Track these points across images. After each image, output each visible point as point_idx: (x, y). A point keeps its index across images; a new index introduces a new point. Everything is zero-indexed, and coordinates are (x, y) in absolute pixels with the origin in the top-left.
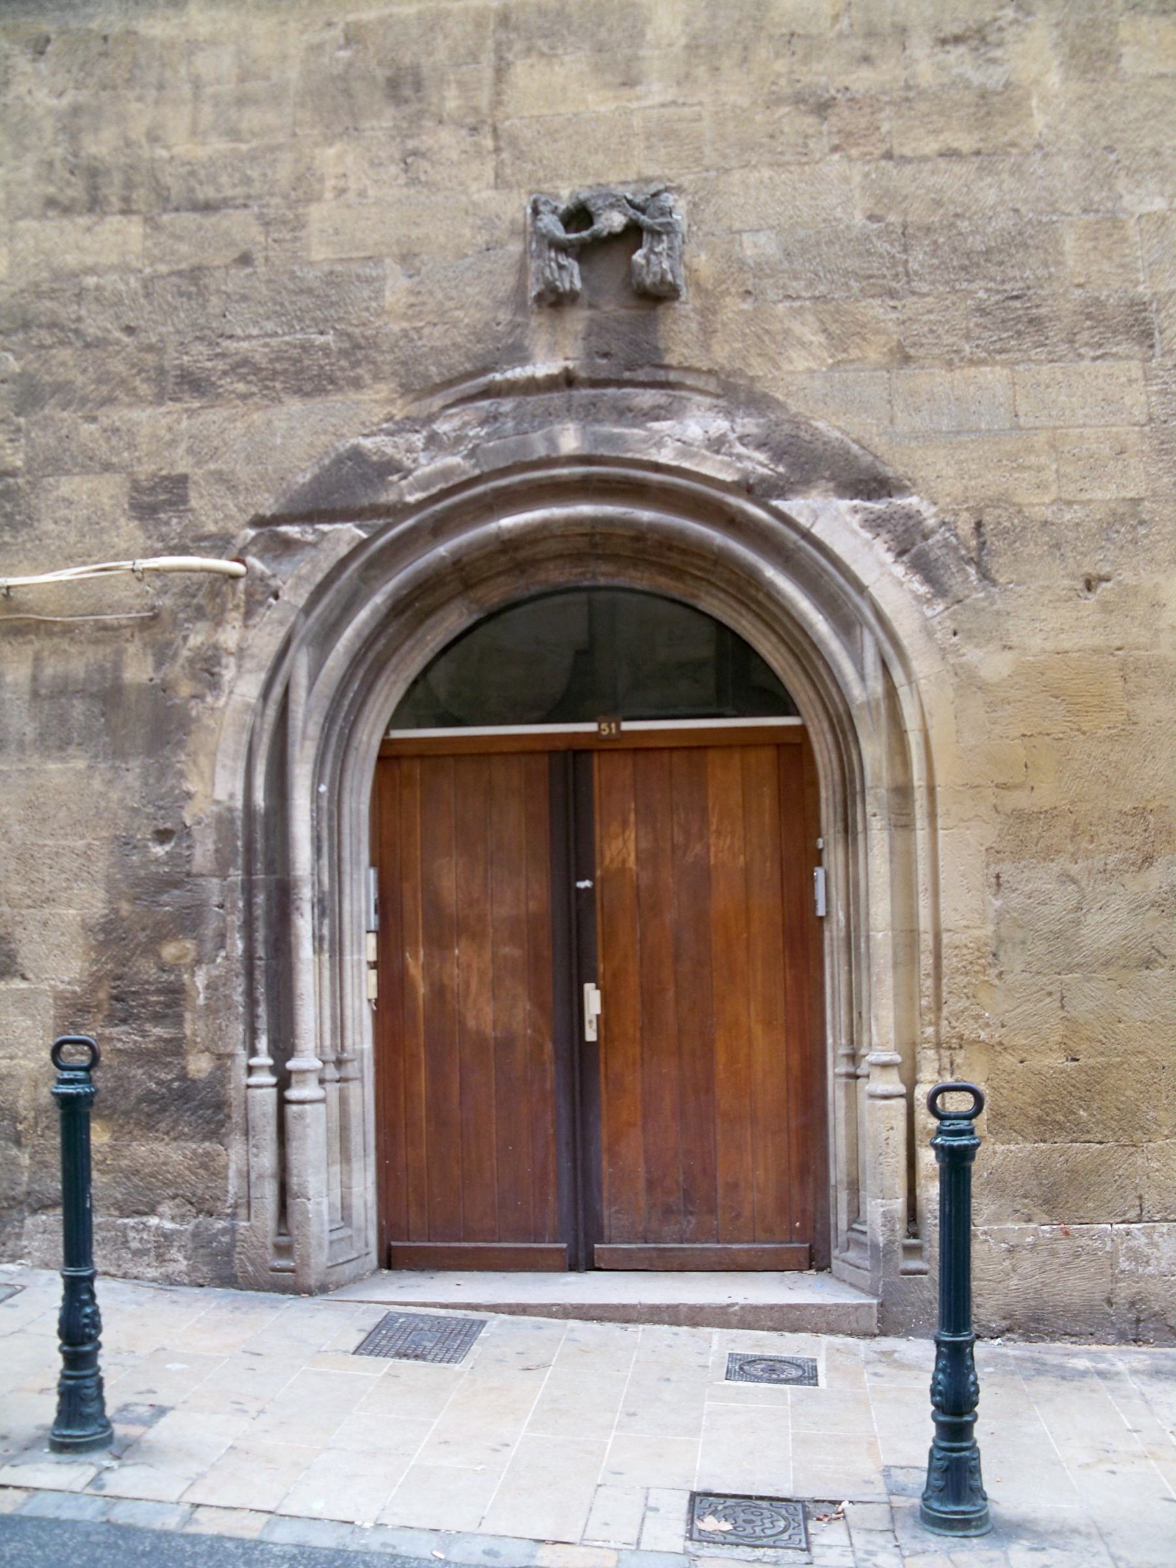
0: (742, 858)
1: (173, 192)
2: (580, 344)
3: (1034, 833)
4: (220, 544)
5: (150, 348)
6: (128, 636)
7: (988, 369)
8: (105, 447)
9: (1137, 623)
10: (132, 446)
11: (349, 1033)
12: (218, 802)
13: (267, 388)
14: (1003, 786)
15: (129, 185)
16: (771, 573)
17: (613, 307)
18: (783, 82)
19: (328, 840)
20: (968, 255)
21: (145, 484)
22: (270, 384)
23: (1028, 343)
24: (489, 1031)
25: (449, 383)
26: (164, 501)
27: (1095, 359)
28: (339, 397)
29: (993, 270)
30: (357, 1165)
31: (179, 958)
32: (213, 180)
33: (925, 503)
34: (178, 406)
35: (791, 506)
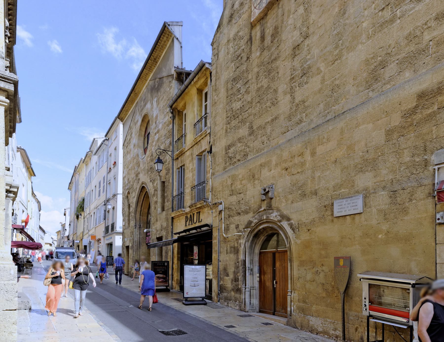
19: (252, 262)
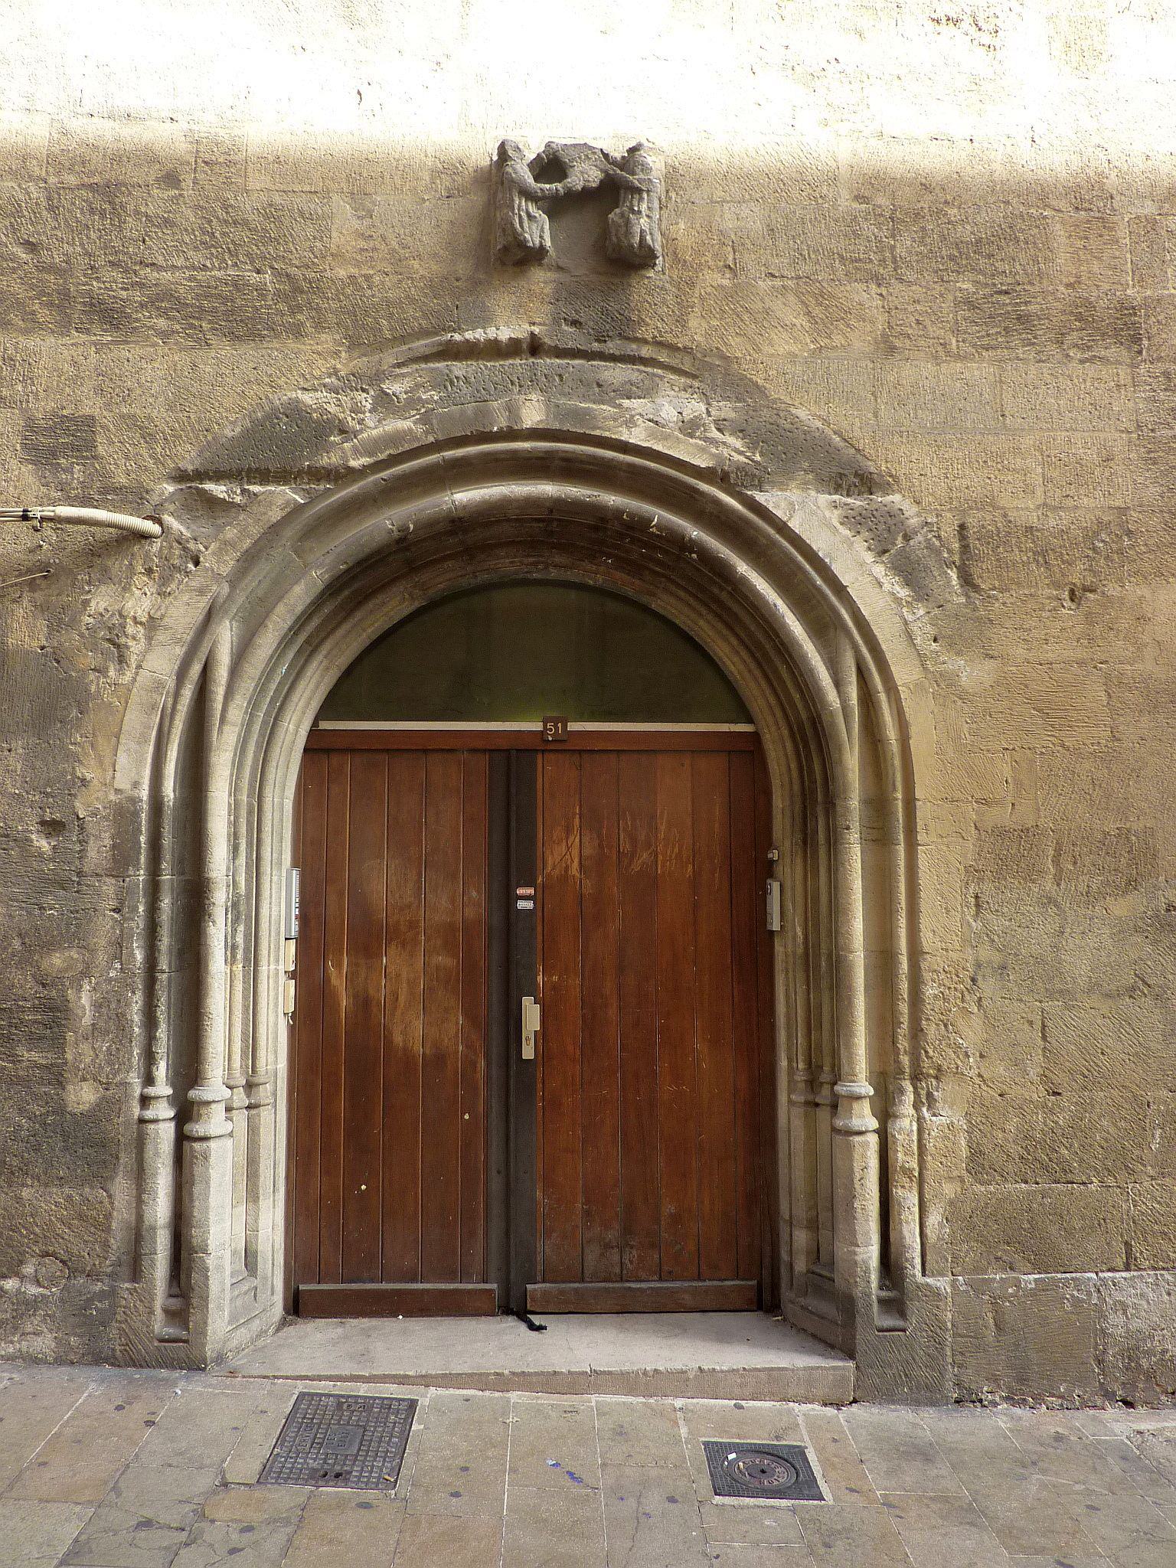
0: (690, 867)
4: (134, 498)
5: (51, 269)
9: (1122, 636)
10: (28, 379)
11: (262, 1053)
12: (118, 791)
13: (192, 326)
14: (984, 802)
16: (743, 568)
25: (403, 339)
27: (1082, 362)
30: (265, 1203)
31: (66, 970)
34: (84, 337)
35: (770, 499)
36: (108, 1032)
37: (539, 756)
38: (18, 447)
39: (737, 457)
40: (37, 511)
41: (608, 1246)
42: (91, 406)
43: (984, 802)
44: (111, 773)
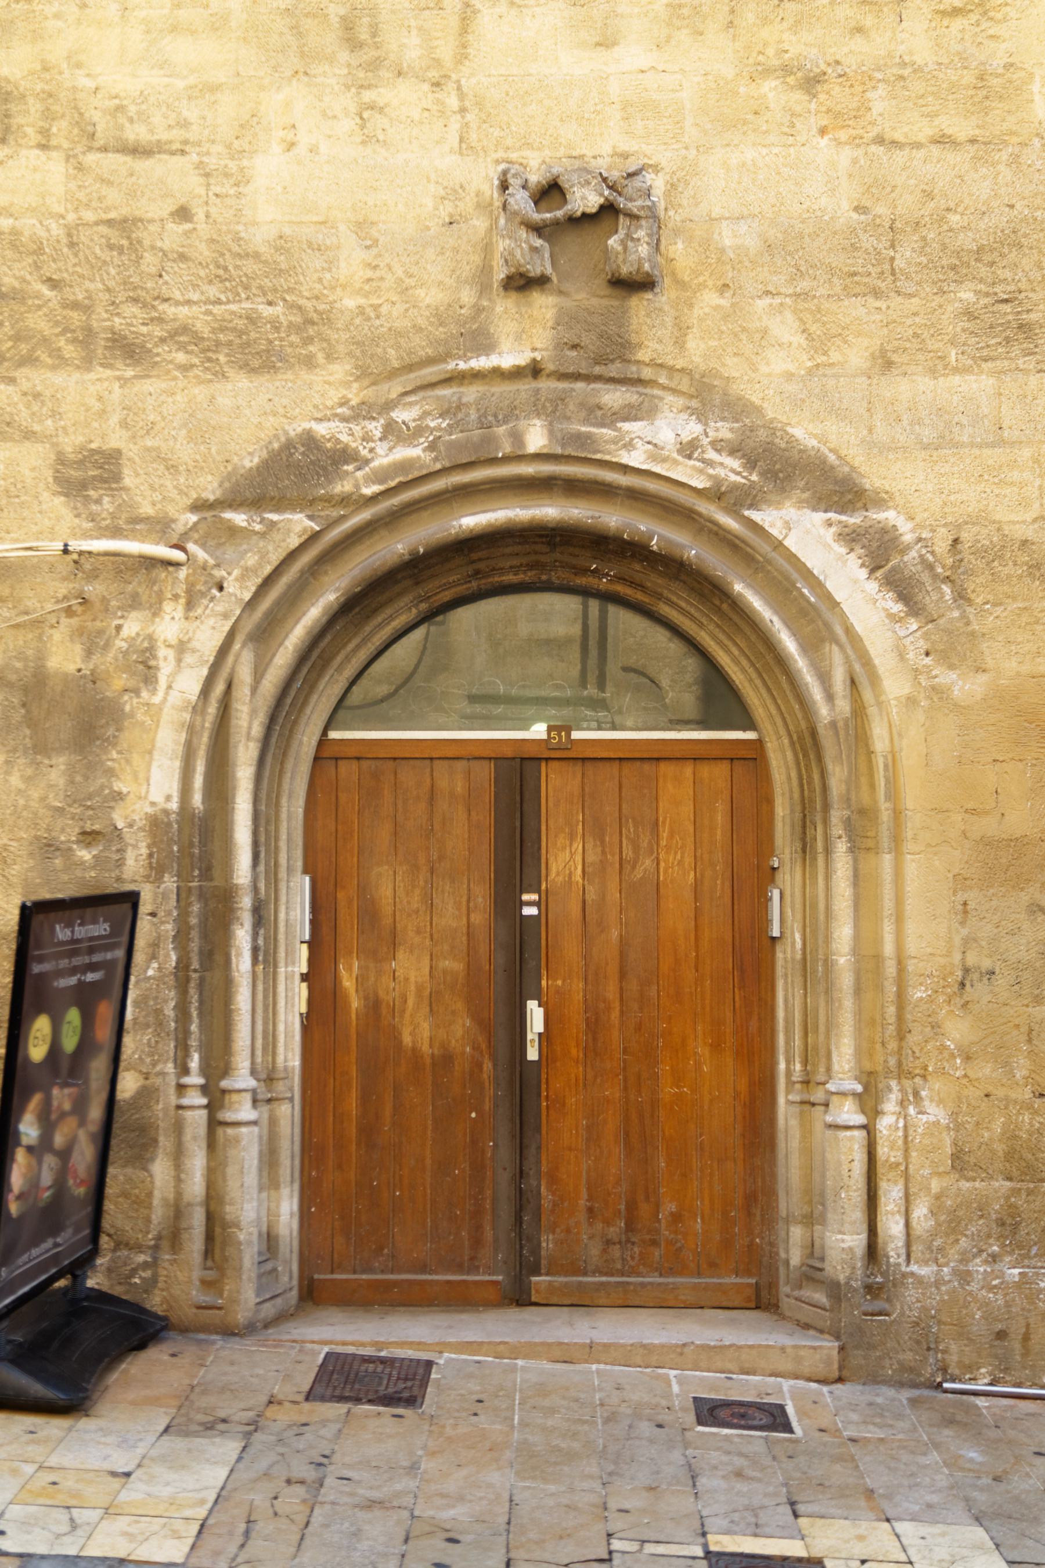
1: (99, 128)
2: (549, 334)
3: (1004, 860)
5: (75, 305)
6: (54, 621)
7: (973, 378)
8: (25, 413)
12: (153, 804)
13: (209, 360)
14: (973, 812)
15: (48, 115)
17: (587, 296)
18: (770, 51)
20: (957, 254)
21: (72, 456)
22: (210, 354)
23: (1016, 350)
24: (425, 1048)
25: (410, 368)
26: (94, 477)
28: (289, 375)
29: (983, 271)
32: (143, 117)
33: (902, 518)
34: (109, 372)
35: (767, 518)
36: (148, 1026)
37: (543, 764)
38: (50, 480)
39: (733, 478)
40: (75, 545)
41: (609, 1242)
42: (116, 440)
43: (973, 812)
44: (145, 787)
